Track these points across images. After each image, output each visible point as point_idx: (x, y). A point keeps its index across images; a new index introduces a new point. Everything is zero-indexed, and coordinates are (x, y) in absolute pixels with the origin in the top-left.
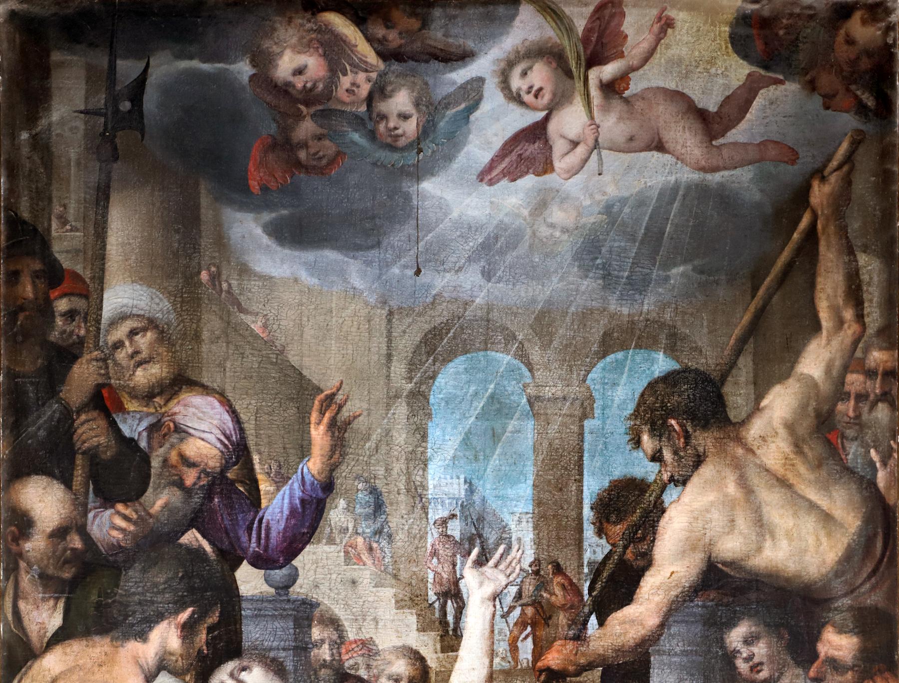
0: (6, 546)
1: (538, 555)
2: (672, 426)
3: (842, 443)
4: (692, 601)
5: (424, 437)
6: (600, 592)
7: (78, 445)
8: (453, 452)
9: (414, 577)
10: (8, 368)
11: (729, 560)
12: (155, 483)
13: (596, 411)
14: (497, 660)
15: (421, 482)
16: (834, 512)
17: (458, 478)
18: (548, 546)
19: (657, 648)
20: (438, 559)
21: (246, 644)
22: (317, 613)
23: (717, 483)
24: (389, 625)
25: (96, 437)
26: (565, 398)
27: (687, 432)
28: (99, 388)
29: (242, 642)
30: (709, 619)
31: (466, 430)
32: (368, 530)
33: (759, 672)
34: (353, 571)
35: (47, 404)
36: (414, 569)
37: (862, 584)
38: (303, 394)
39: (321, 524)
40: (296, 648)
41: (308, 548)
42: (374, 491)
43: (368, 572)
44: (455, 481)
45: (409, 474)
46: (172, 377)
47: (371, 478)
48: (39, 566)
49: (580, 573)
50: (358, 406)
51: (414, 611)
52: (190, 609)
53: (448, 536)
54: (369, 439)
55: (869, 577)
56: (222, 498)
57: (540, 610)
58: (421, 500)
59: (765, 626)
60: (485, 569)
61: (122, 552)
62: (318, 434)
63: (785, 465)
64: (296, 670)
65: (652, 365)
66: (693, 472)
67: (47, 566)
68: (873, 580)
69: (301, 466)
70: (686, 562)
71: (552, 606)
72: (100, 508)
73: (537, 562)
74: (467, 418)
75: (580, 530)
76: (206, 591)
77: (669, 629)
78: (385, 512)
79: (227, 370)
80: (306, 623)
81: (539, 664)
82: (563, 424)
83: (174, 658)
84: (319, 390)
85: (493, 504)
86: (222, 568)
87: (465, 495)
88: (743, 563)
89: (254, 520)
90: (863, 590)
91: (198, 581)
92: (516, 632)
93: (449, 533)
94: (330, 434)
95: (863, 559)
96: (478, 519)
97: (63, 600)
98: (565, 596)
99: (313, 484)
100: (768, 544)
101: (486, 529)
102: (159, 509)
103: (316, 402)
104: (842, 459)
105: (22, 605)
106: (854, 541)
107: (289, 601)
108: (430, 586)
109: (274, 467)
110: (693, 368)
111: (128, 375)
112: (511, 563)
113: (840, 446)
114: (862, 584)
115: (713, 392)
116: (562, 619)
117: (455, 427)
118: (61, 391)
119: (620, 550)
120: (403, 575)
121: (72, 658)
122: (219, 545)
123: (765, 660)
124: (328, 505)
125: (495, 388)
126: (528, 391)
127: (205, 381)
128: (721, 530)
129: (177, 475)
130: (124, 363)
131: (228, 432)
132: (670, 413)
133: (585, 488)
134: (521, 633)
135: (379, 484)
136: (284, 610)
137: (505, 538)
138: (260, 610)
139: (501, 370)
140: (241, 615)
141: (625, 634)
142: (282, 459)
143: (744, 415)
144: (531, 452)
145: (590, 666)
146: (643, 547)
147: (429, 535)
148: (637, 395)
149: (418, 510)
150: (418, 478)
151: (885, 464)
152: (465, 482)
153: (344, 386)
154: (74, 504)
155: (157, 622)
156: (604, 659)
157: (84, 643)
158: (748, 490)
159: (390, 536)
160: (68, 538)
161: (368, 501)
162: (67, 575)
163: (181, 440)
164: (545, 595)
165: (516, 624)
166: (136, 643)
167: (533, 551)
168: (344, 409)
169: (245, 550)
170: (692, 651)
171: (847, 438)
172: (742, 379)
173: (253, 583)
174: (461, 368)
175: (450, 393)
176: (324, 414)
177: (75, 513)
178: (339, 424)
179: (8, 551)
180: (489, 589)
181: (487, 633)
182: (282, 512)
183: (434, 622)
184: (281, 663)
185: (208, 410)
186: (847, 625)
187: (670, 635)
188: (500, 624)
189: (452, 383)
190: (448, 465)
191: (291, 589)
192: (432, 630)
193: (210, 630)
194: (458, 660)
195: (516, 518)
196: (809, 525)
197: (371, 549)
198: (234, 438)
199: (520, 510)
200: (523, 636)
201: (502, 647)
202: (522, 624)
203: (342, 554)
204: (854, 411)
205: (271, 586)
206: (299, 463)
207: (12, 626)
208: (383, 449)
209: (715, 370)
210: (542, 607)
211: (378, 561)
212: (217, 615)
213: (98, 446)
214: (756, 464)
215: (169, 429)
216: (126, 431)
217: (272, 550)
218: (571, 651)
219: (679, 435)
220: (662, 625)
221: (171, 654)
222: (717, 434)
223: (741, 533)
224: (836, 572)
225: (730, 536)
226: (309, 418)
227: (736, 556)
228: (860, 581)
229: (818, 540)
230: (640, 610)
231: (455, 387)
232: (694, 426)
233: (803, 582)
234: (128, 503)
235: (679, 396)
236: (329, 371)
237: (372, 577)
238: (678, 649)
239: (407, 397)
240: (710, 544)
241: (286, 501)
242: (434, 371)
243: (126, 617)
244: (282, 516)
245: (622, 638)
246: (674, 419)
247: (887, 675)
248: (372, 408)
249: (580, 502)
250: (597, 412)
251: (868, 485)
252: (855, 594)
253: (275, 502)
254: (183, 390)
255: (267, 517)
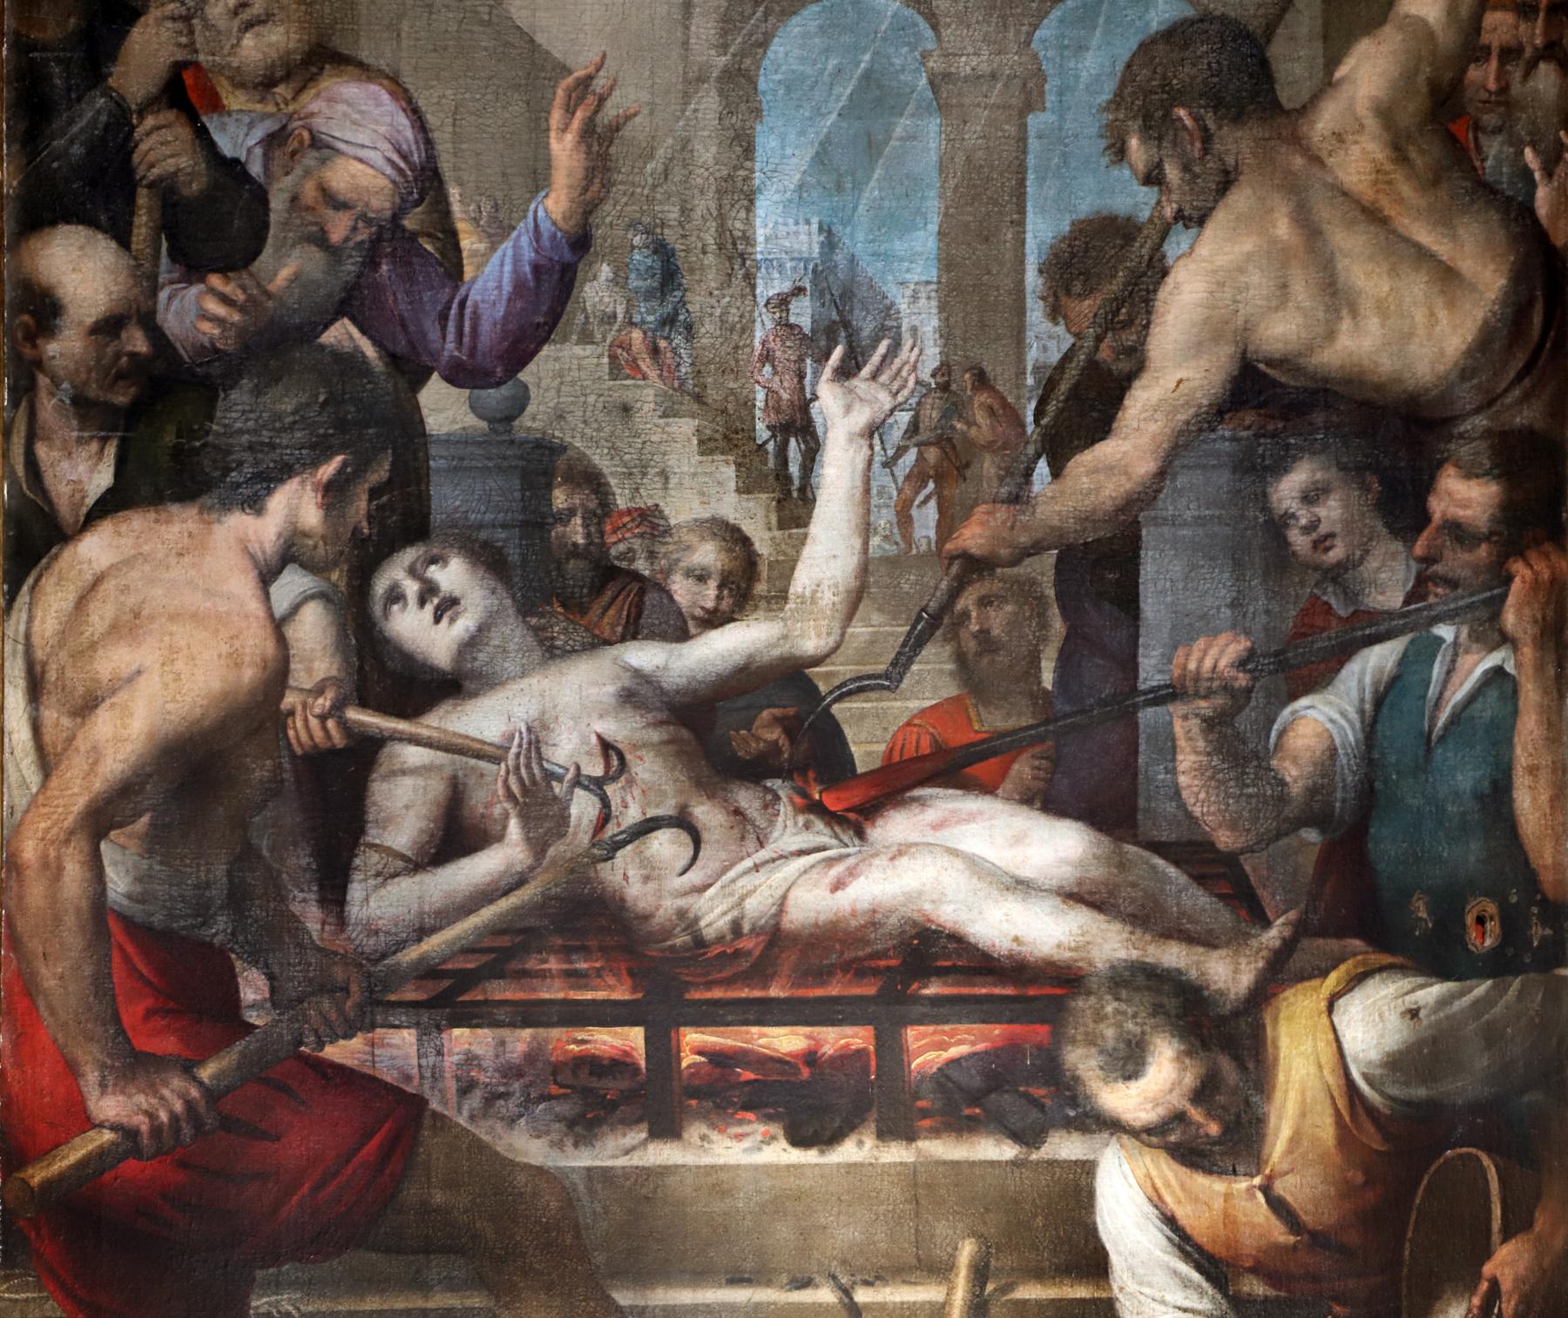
0: (13, 348)
1: (947, 356)
2: (1180, 119)
3: (1476, 139)
4: (1213, 430)
5: (749, 151)
6: (1056, 418)
7: (141, 172)
8: (798, 176)
9: (731, 398)
10: (17, 34)
11: (1277, 356)
12: (276, 237)
13: (1047, 97)
14: (875, 541)
15: (744, 232)
16: (1460, 263)
17: (808, 222)
18: (965, 340)
19: (1153, 513)
20: (774, 367)
21: (437, 518)
22: (561, 463)
23: (1258, 221)
24: (687, 481)
25: (172, 156)
26: (994, 76)
27: (1205, 129)
28: (178, 68)
29: (429, 514)
30: (1242, 461)
31: (822, 137)
32: (651, 318)
33: (1327, 549)
34: (626, 390)
35: (86, 98)
36: (732, 385)
37: (1506, 390)
38: (537, 78)
39: (569, 308)
40: (524, 524)
41: (546, 350)
42: (662, 250)
43: (651, 392)
44: (803, 228)
45: (722, 218)
46: (306, 48)
47: (656, 226)
48: (71, 383)
49: (1019, 385)
50: (632, 97)
51: (731, 458)
52: (339, 459)
53: (791, 326)
54: (652, 157)
55: (1519, 378)
56: (394, 263)
57: (951, 453)
58: (744, 264)
59: (1341, 469)
60: (855, 382)
61: (219, 359)
62: (564, 149)
63: (1375, 183)
64: (525, 562)
65: (1147, 10)
66: (1216, 201)
67: (86, 383)
68: (1527, 382)
69: (532, 206)
70: (1204, 363)
71: (970, 443)
72: (179, 282)
73: (944, 369)
74: (823, 116)
75: (1021, 311)
76: (368, 427)
77: (1173, 480)
78: (680, 285)
79: (403, 35)
80: (543, 480)
81: (949, 546)
82: (991, 122)
83: (311, 542)
84: (566, 70)
85: (869, 267)
86: (396, 384)
87: (821, 254)
88: (1301, 361)
89: (450, 302)
90: (1508, 400)
91: (353, 409)
92: (908, 492)
93: (792, 320)
94: (583, 148)
95: (1510, 346)
96: (841, 297)
97: (115, 443)
98: (993, 428)
99: (554, 236)
100: (1346, 325)
101: (856, 312)
102: (284, 284)
103: (560, 92)
104: (1474, 169)
105: (41, 450)
106: (1494, 314)
107: (512, 442)
108: (758, 413)
109: (487, 208)
110: (1218, 13)
111: (228, 47)
112: (900, 370)
113: (1472, 146)
114: (1506, 390)
115: (1252, 56)
116: (988, 466)
117: (802, 133)
118: (111, 74)
119: (1088, 344)
120: (713, 395)
121: (130, 541)
122: (390, 347)
123: (1338, 529)
124: (580, 275)
125: (872, 60)
126: (931, 64)
127: (365, 55)
128: (1264, 303)
129: (316, 224)
130: (222, 24)
131: (405, 147)
132: (1178, 97)
133: (1029, 236)
134: (917, 493)
135: (670, 236)
136: (505, 458)
137: (889, 328)
138: (461, 459)
139: (883, 28)
140: (428, 468)
141: (1098, 490)
142: (499, 195)
143: (1305, 96)
144: (935, 174)
145: (1036, 549)
146: (1129, 338)
147: (758, 325)
148: (1120, 67)
149: (738, 281)
150: (738, 225)
151: (1549, 174)
152: (821, 229)
153: (607, 61)
154: (134, 276)
155: (281, 481)
156: (1061, 536)
157: (152, 515)
158: (1310, 230)
159: (689, 328)
160: (124, 335)
161: (651, 267)
162: (121, 399)
163: (324, 161)
164: (959, 426)
165: (908, 478)
166: (244, 517)
167: (937, 350)
168: (609, 103)
169: (435, 356)
170: (1212, 517)
171: (1484, 131)
172: (1303, 30)
173: (450, 413)
174: (813, 26)
175: (793, 72)
176: (573, 113)
177: (136, 291)
178: (599, 130)
179: (17, 357)
180: (861, 417)
181: (858, 494)
182: (499, 287)
183: (767, 476)
184: (500, 551)
185: (369, 107)
186: (1481, 464)
187: (1175, 490)
188: (881, 478)
189: (796, 52)
190: (790, 201)
191: (516, 423)
192: (762, 490)
193: (374, 493)
194: (809, 541)
195: (909, 292)
196: (1416, 290)
197: (655, 351)
198: (416, 158)
199: (916, 278)
200: (921, 498)
201: (884, 518)
202: (918, 477)
203: (606, 360)
204: (1498, 79)
205: (480, 417)
206: (530, 200)
207: (24, 487)
208: (677, 174)
209: (1255, 16)
210: (954, 447)
211: (668, 372)
212: (387, 467)
213: (175, 174)
214: (1325, 184)
215: (301, 142)
216: (226, 146)
217: (484, 354)
218: (1004, 522)
219: (1191, 135)
220: (1161, 474)
221: (305, 535)
222: (1258, 131)
223: (1298, 308)
224: (1463, 370)
225: (1281, 314)
226: (547, 120)
227: (1289, 347)
228: (1503, 385)
229: (1432, 314)
230: (1123, 449)
231: (802, 60)
232: (1219, 120)
233: (1405, 391)
234: (230, 274)
235: (1194, 65)
236: (581, 36)
237: (659, 399)
238: (1188, 515)
239: (719, 79)
240: (1246, 329)
241: (508, 268)
242: (764, 34)
243: (227, 471)
244: (500, 294)
245: (1092, 498)
246: (1183, 106)
247: (1548, 547)
248: (658, 101)
249: (1020, 261)
250: (1051, 99)
251: (1518, 214)
252: (1494, 409)
253: (487, 269)
254: (326, 73)
255: (474, 296)
